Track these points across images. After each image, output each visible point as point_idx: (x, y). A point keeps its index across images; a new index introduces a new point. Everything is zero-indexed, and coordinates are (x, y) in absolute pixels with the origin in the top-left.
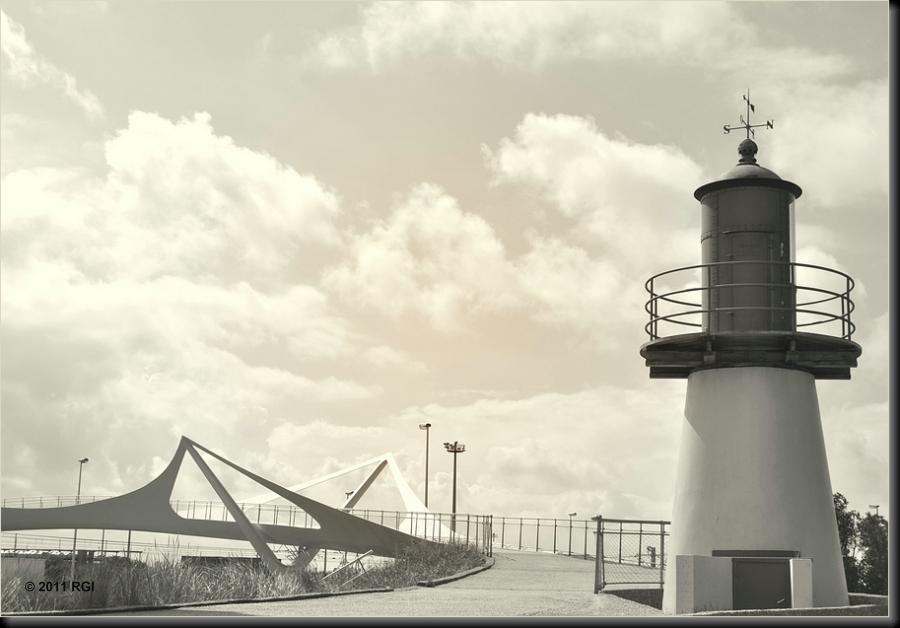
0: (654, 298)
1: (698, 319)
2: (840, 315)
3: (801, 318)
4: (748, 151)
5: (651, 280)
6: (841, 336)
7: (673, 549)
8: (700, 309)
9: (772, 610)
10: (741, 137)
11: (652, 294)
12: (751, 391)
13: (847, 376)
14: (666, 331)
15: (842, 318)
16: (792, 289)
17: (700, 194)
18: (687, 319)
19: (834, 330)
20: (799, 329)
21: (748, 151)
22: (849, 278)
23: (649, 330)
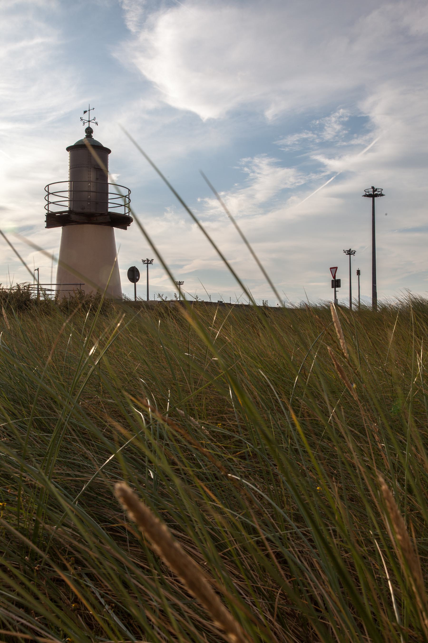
0: (49, 203)
1: (67, 204)
2: (123, 204)
3: (110, 205)
4: (89, 131)
5: (48, 186)
6: (124, 213)
7: (281, 627)
8: (68, 199)
9: (261, 372)
10: (87, 125)
11: (48, 202)
12: (89, 231)
13: (126, 229)
14: (54, 209)
15: (124, 206)
16: (107, 193)
17: (68, 149)
18: (63, 205)
19: (121, 211)
20: (110, 210)
21: (89, 131)
22: (129, 190)
23: (47, 208)
